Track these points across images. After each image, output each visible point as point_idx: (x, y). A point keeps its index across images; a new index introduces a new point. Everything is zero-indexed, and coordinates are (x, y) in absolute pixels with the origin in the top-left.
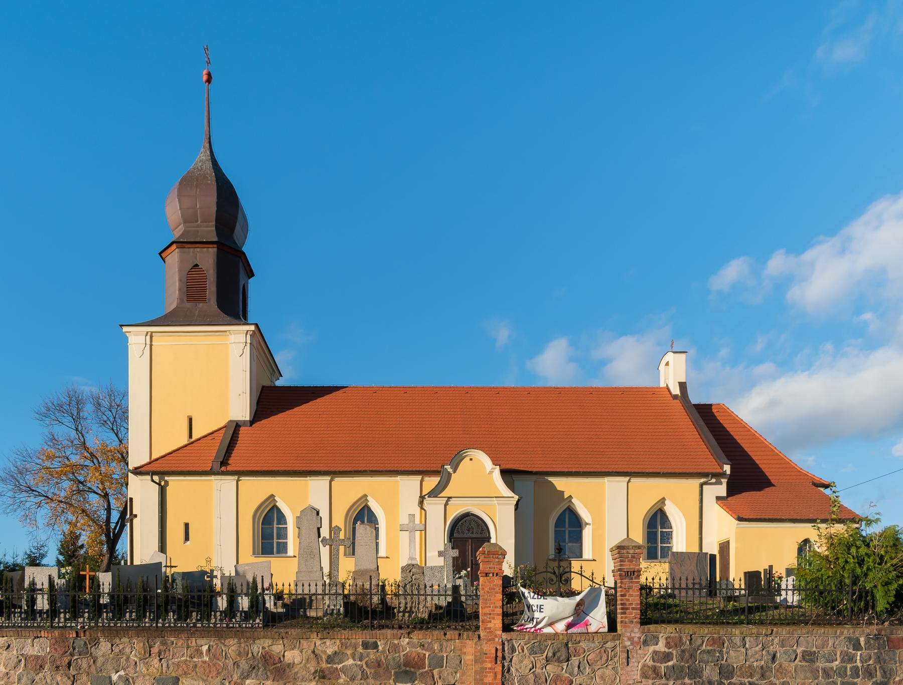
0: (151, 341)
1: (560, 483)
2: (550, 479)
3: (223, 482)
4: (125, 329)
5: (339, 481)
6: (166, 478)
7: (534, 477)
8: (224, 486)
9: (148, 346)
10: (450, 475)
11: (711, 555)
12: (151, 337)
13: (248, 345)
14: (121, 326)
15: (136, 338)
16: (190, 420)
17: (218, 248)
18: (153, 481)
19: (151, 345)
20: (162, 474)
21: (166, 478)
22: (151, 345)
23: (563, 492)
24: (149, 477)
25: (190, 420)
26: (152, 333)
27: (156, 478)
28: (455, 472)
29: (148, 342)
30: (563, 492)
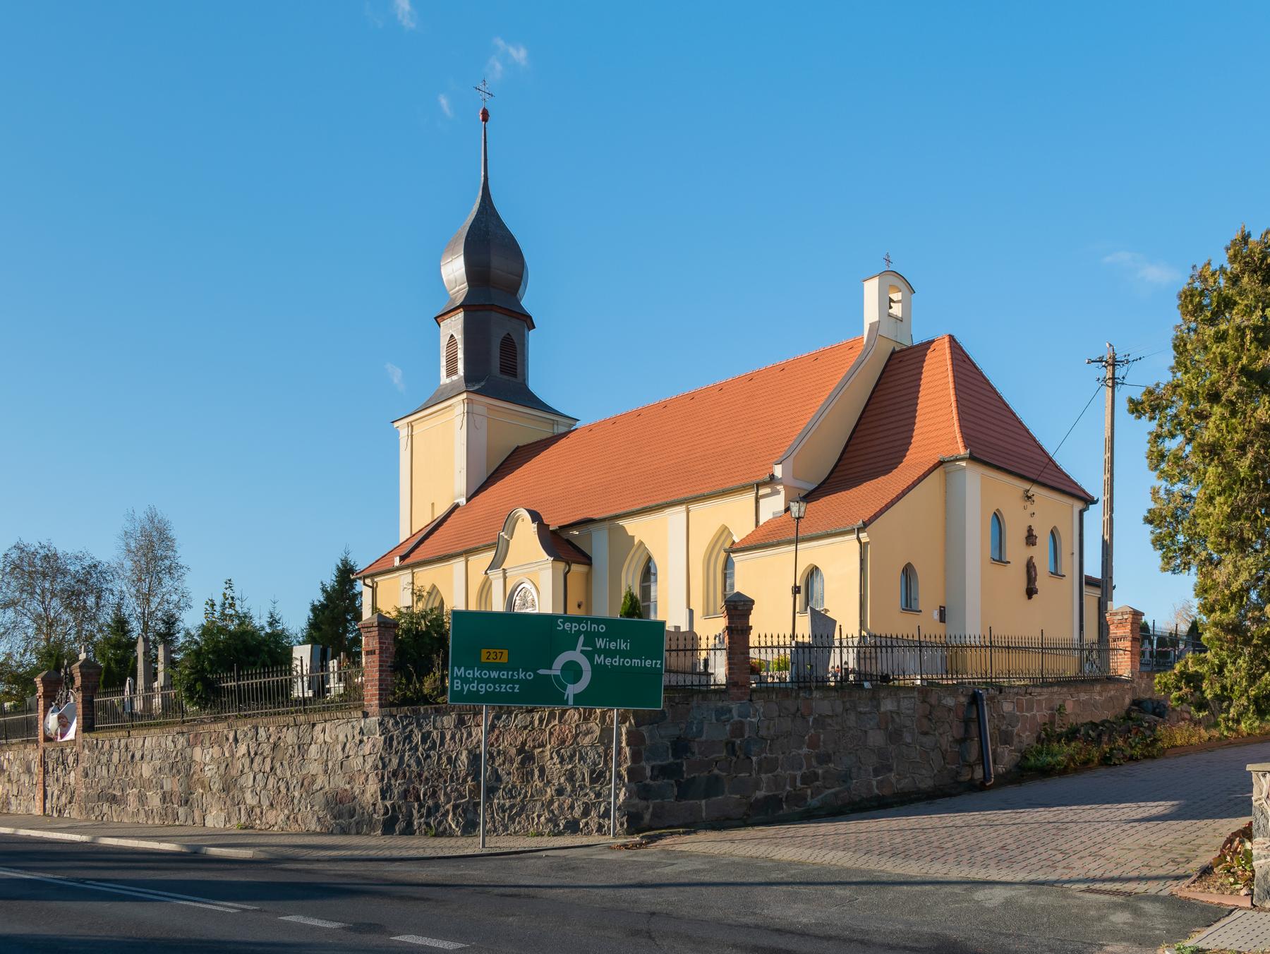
2: (621, 523)
4: (396, 425)
5: (696, 509)
7: (607, 524)
15: (402, 428)
27: (368, 581)
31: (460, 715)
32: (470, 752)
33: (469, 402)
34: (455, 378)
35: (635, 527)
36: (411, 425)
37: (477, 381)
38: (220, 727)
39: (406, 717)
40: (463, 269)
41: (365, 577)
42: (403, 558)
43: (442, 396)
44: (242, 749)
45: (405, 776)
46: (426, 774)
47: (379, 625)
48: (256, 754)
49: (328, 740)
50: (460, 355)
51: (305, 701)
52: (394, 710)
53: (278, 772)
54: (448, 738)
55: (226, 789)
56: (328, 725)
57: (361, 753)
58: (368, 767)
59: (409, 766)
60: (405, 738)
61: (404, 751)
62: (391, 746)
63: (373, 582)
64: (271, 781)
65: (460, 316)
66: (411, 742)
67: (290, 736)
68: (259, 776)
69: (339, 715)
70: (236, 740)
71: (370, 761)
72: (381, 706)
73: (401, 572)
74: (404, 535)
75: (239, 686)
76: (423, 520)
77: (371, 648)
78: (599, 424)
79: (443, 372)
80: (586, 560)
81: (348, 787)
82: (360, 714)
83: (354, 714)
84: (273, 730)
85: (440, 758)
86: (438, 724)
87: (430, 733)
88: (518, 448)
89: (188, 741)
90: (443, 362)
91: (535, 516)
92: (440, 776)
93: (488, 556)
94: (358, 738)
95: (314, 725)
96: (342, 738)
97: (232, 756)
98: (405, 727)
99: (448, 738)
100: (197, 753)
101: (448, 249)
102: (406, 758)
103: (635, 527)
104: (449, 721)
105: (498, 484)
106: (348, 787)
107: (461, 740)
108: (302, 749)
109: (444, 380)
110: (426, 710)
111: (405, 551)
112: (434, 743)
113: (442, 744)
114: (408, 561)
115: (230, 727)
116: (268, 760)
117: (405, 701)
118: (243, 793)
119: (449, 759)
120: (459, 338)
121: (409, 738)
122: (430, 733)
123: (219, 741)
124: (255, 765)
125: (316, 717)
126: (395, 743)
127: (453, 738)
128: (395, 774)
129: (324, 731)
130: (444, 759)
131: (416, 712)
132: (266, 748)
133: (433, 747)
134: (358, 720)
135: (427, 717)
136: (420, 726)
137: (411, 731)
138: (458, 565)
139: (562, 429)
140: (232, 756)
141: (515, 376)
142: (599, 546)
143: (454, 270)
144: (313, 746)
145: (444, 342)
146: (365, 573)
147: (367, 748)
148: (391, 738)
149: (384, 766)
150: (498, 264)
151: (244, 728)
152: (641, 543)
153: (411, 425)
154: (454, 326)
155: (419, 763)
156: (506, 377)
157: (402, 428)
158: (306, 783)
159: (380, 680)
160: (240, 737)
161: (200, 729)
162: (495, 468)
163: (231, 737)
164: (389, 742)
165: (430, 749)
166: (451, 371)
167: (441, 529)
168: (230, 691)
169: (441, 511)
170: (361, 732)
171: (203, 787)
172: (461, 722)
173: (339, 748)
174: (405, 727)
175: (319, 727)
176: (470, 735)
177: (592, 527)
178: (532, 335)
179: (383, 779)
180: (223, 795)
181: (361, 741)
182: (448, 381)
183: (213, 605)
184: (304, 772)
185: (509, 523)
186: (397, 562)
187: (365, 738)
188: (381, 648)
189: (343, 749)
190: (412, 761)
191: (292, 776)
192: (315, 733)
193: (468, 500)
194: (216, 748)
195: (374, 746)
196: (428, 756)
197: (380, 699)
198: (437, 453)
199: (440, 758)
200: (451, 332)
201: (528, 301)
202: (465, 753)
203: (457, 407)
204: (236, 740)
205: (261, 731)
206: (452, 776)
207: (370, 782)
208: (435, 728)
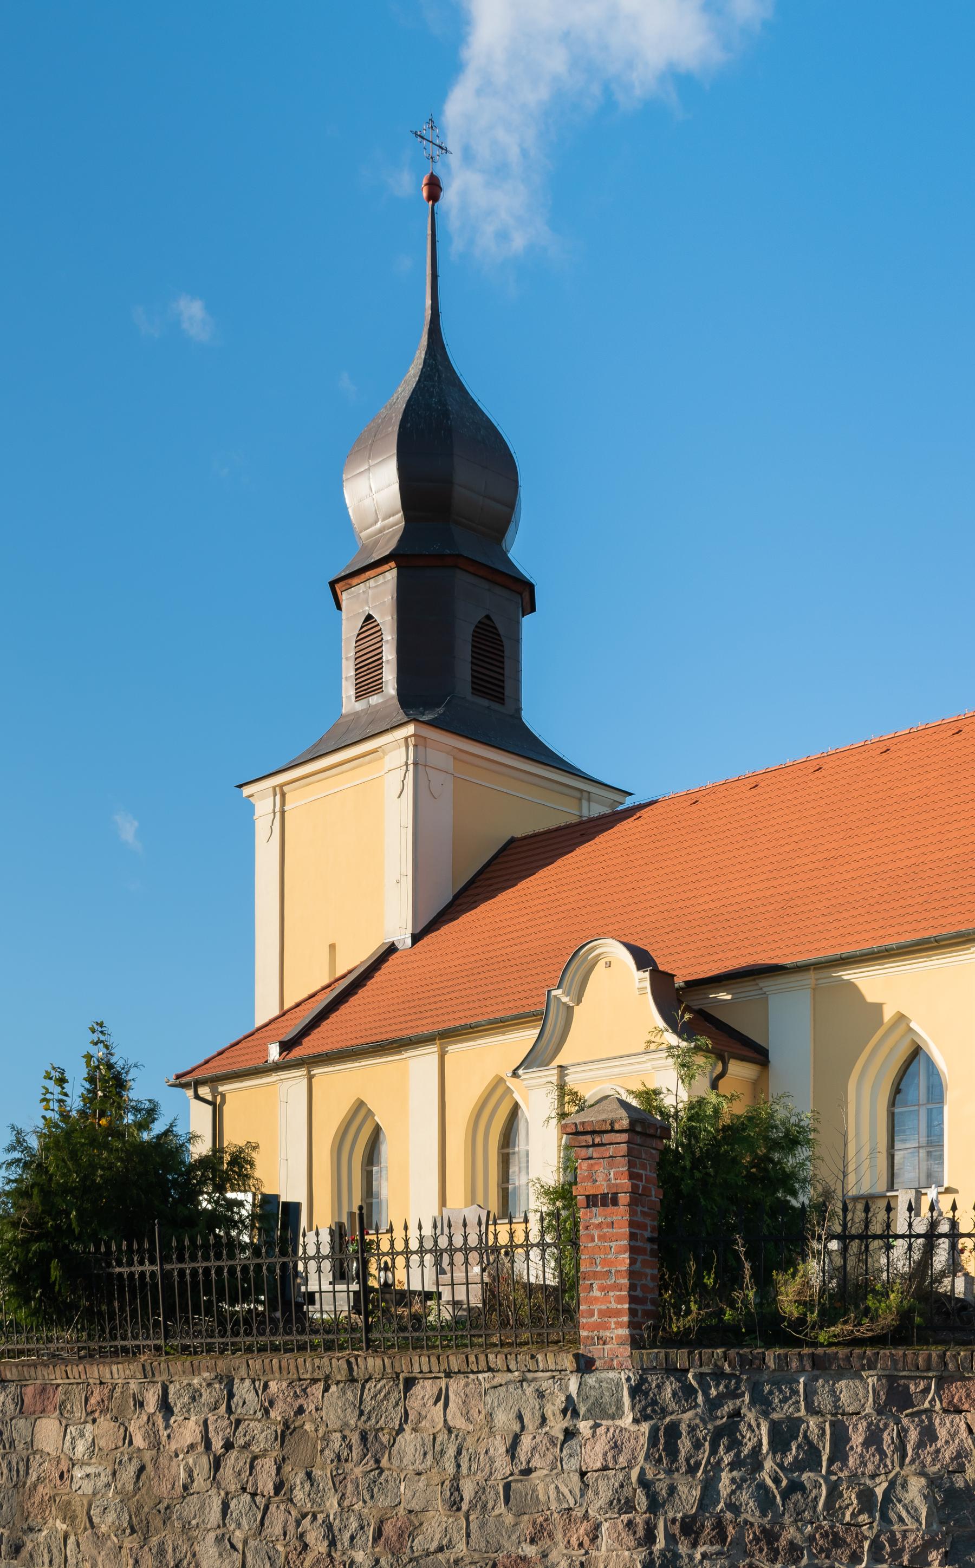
1: (875, 983)
2: (848, 975)
3: (290, 1083)
4: (247, 791)
5: (458, 1051)
7: (810, 978)
8: (292, 1085)
9: (278, 815)
10: (570, 1010)
11: (286, 1205)
12: (283, 795)
13: (411, 767)
14: (240, 786)
15: (262, 798)
17: (398, 566)
18: (197, 1097)
20: (214, 1081)
21: (221, 1089)
22: (283, 813)
23: (878, 1007)
27: (204, 1091)
28: (579, 1002)
30: (878, 1007)
31: (891, 1379)
32: (933, 1482)
33: (420, 742)
34: (375, 700)
35: (883, 986)
36: (281, 793)
37: (429, 705)
38: (119, 1373)
39: (719, 1375)
40: (396, 487)
41: (198, 1083)
42: (286, 1046)
43: (345, 736)
44: (187, 1431)
45: (721, 1536)
46: (791, 1533)
47: (631, 1130)
48: (228, 1446)
49: (457, 1421)
50: (389, 654)
51: (332, 1327)
52: (680, 1357)
53: (299, 1495)
54: (857, 1439)
55: (138, 1527)
56: (456, 1387)
57: (572, 1465)
58: (597, 1504)
59: (734, 1508)
60: (717, 1436)
61: (717, 1467)
62: (672, 1451)
63: (214, 1092)
64: (278, 1518)
65: (389, 578)
66: (735, 1444)
67: (332, 1409)
68: (240, 1504)
69: (496, 1360)
70: (166, 1407)
71: (604, 1490)
72: (636, 1343)
73: (284, 1075)
74: (265, 1009)
75: (167, 1275)
76: (310, 978)
77: (602, 1187)
78: (714, 790)
79: (348, 689)
80: (758, 1055)
81: (530, 1551)
82: (568, 1362)
83: (547, 1359)
84: (264, 1385)
85: (834, 1492)
86: (823, 1400)
87: (794, 1424)
88: (512, 840)
89: (20, 1401)
90: (348, 670)
91: (642, 959)
92: (837, 1541)
93: (526, 1037)
94: (557, 1426)
95: (410, 1383)
96: (505, 1419)
97: (156, 1445)
98: (713, 1405)
99: (857, 1439)
100: (48, 1432)
101: (361, 448)
102: (725, 1483)
103: (883, 986)
104: (857, 1393)
105: (484, 907)
106: (530, 1551)
107: (901, 1449)
108: (372, 1443)
109: (349, 703)
110: (783, 1361)
111: (290, 1029)
112: (813, 1453)
113: (839, 1452)
114: (297, 1053)
115: (148, 1374)
116: (267, 1466)
117: (710, 1335)
118: (192, 1541)
119: (866, 1497)
120: (387, 622)
121: (728, 1433)
122: (794, 1424)
123: (116, 1408)
124: (227, 1473)
125: (420, 1362)
126: (685, 1445)
127: (873, 1439)
128: (690, 1528)
129: (442, 1398)
130: (851, 1496)
131: (753, 1365)
132: (261, 1434)
133: (811, 1459)
134: (558, 1375)
135: (784, 1378)
136: (762, 1403)
137: (737, 1413)
138: (421, 1064)
139: (597, 810)
140: (156, 1445)
141: (501, 700)
142: (788, 1021)
143: (374, 493)
144: (408, 1435)
145: (350, 627)
146: (197, 1075)
147: (594, 1455)
148: (673, 1432)
149: (654, 1505)
150: (468, 482)
151: (191, 1379)
152: (901, 1018)
153: (281, 793)
154: (378, 597)
155: (765, 1500)
156: (485, 702)
157: (262, 798)
158: (388, 1529)
159: (632, 1274)
160: (178, 1400)
161: (56, 1375)
162: (470, 879)
163: (152, 1399)
164: (665, 1441)
165: (799, 1466)
166: (367, 684)
167: (362, 993)
168: (138, 1286)
169: (354, 957)
170: (570, 1409)
171: (68, 1515)
172: (896, 1398)
173: (499, 1447)
174: (713, 1405)
175: (424, 1390)
176: (928, 1434)
177: (768, 985)
178: (527, 622)
179: (650, 1538)
180: (130, 1542)
181: (570, 1434)
182: (359, 706)
183: (62, 1081)
184: (384, 1502)
185: (575, 968)
186: (274, 1052)
187: (584, 1426)
188: (634, 1192)
189: (512, 1450)
190: (745, 1497)
191: (345, 1510)
192: (414, 1403)
193: (416, 938)
194: (105, 1424)
195: (616, 1447)
196: (796, 1487)
197: (632, 1325)
198: (346, 845)
199: (834, 1492)
200: (367, 610)
201: (524, 551)
202: (916, 1485)
203: (394, 752)
204: (166, 1407)
205: (243, 1390)
206: (876, 1546)
207: (605, 1540)
208: (812, 1410)
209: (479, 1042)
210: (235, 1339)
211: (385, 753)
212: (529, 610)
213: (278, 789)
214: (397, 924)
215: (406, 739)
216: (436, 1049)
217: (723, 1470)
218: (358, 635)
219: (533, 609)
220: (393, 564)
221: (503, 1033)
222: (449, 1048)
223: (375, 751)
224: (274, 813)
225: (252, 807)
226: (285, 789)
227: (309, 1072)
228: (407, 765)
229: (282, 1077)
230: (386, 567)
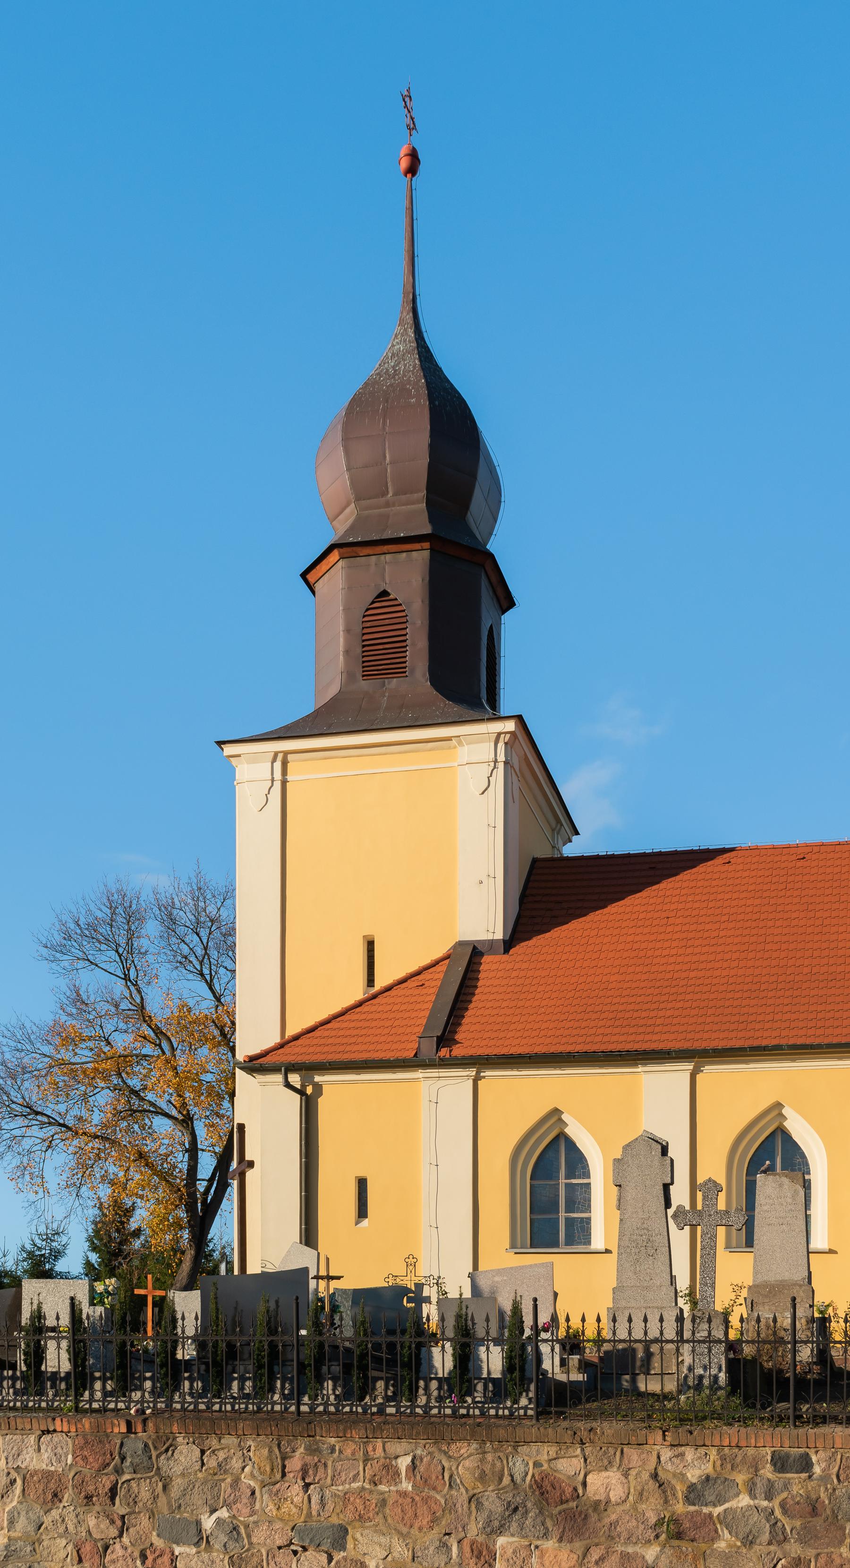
0: (284, 772)
4: (229, 750)
6: (317, 1079)
9: (278, 785)
12: (285, 764)
13: (501, 766)
16: (370, 945)
19: (284, 783)
20: (308, 1068)
21: (317, 1079)
22: (284, 783)
24: (279, 1078)
25: (370, 945)
26: (286, 754)
27: (295, 1079)
29: (278, 775)
65: (421, 556)
178: (508, 618)
209: (752, 1065)
210: (391, 1339)
211: (460, 743)
212: (505, 605)
213: (280, 756)
214: (483, 915)
215: (499, 734)
216: (691, 1067)
217: (194, 1339)
218: (367, 610)
219: (511, 604)
220: (427, 545)
221: (793, 1060)
222: (706, 1067)
223: (449, 739)
224: (273, 780)
225: (233, 770)
226: (290, 757)
227: (478, 1073)
228: (496, 761)
229: (441, 1075)
230: (417, 546)
